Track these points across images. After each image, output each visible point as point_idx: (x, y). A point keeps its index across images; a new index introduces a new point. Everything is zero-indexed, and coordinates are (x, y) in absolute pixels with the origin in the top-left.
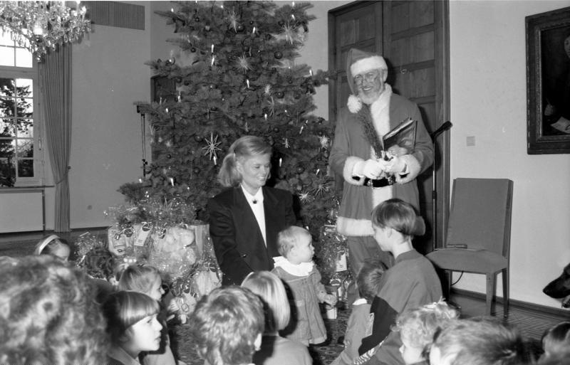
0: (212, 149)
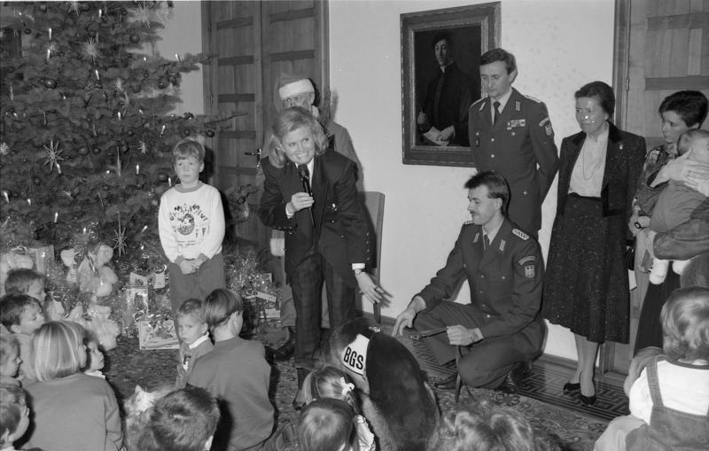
0: (53, 158)
